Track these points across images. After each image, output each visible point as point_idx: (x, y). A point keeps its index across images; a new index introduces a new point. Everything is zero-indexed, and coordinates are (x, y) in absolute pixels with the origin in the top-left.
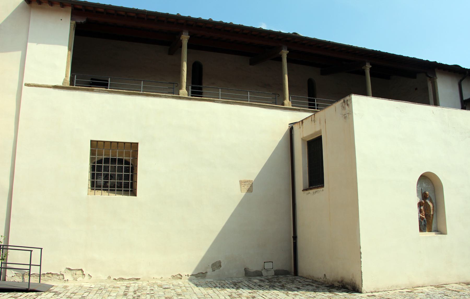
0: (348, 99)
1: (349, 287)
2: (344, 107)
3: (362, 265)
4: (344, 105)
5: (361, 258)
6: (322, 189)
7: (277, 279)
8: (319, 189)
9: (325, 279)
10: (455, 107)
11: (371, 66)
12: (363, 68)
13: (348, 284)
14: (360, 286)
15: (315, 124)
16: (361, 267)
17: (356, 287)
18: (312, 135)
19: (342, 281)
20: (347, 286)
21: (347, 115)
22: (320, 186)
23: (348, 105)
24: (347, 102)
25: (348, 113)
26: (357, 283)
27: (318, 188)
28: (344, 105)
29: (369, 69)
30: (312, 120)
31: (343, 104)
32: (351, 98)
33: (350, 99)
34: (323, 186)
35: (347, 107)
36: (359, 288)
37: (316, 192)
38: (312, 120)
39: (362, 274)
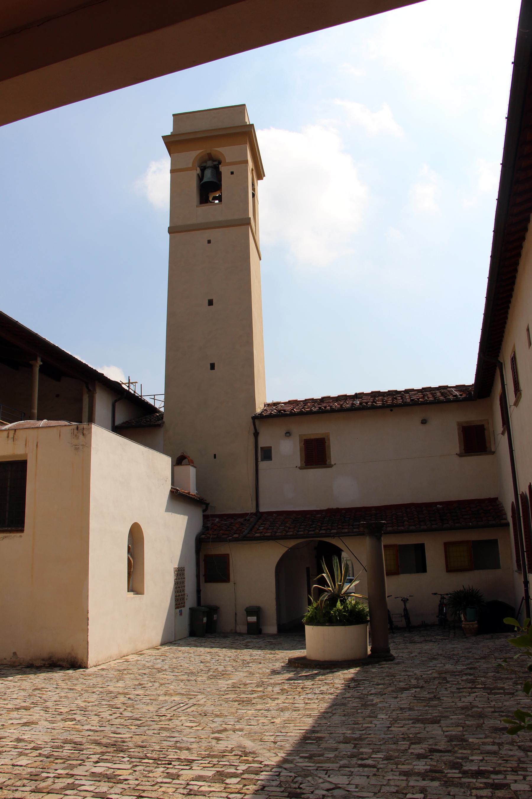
0: (84, 428)
1: (64, 664)
2: (76, 436)
3: (89, 634)
4: (77, 433)
5: (88, 625)
6: (18, 535)
7: (217, 682)
8: (12, 535)
9: (14, 659)
10: (106, 427)
11: (42, 363)
12: (30, 362)
13: (63, 660)
14: (85, 659)
15: (14, 444)
16: (88, 636)
17: (77, 663)
18: (10, 456)
19: (50, 658)
20: (61, 663)
21: (81, 447)
22: (9, 529)
23: (83, 434)
24: (83, 431)
25: (83, 445)
26: (79, 656)
27: (10, 533)
28: (77, 433)
29: (38, 366)
30: (8, 437)
31: (76, 431)
32: (91, 428)
33: (89, 429)
34: (22, 531)
35: (81, 436)
36: (83, 662)
37: (6, 537)
38: (8, 437)
39: (88, 645)
